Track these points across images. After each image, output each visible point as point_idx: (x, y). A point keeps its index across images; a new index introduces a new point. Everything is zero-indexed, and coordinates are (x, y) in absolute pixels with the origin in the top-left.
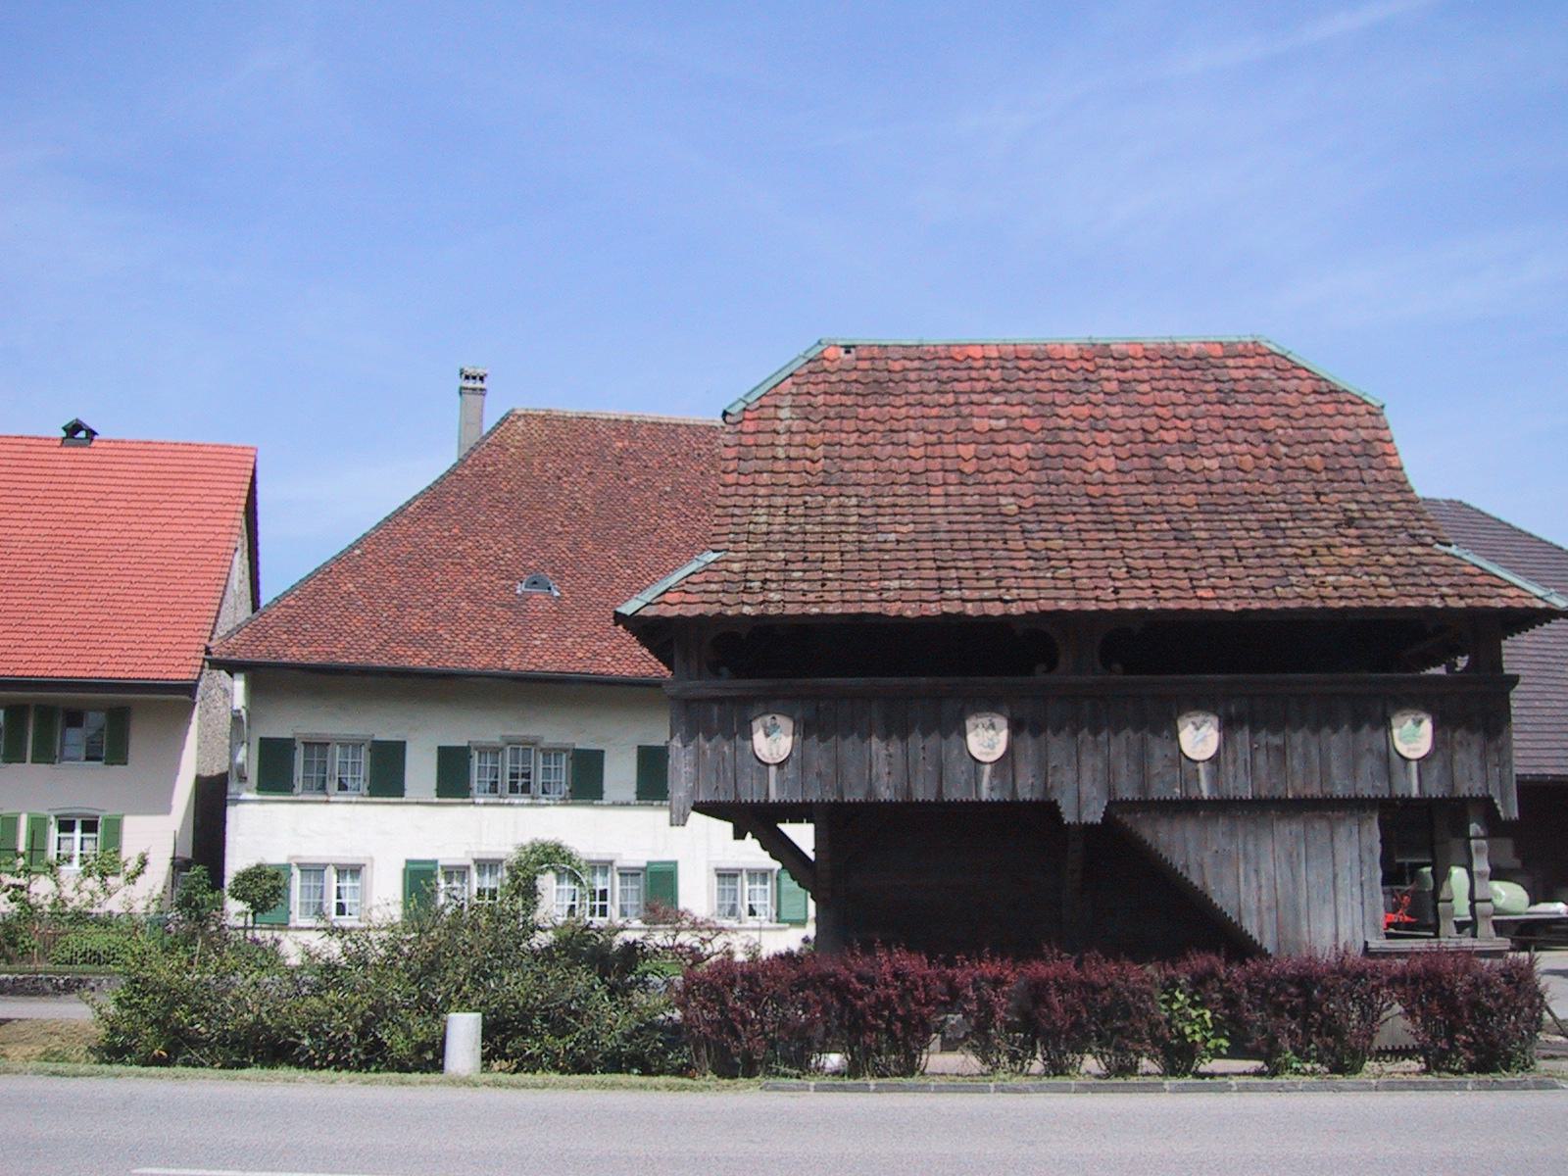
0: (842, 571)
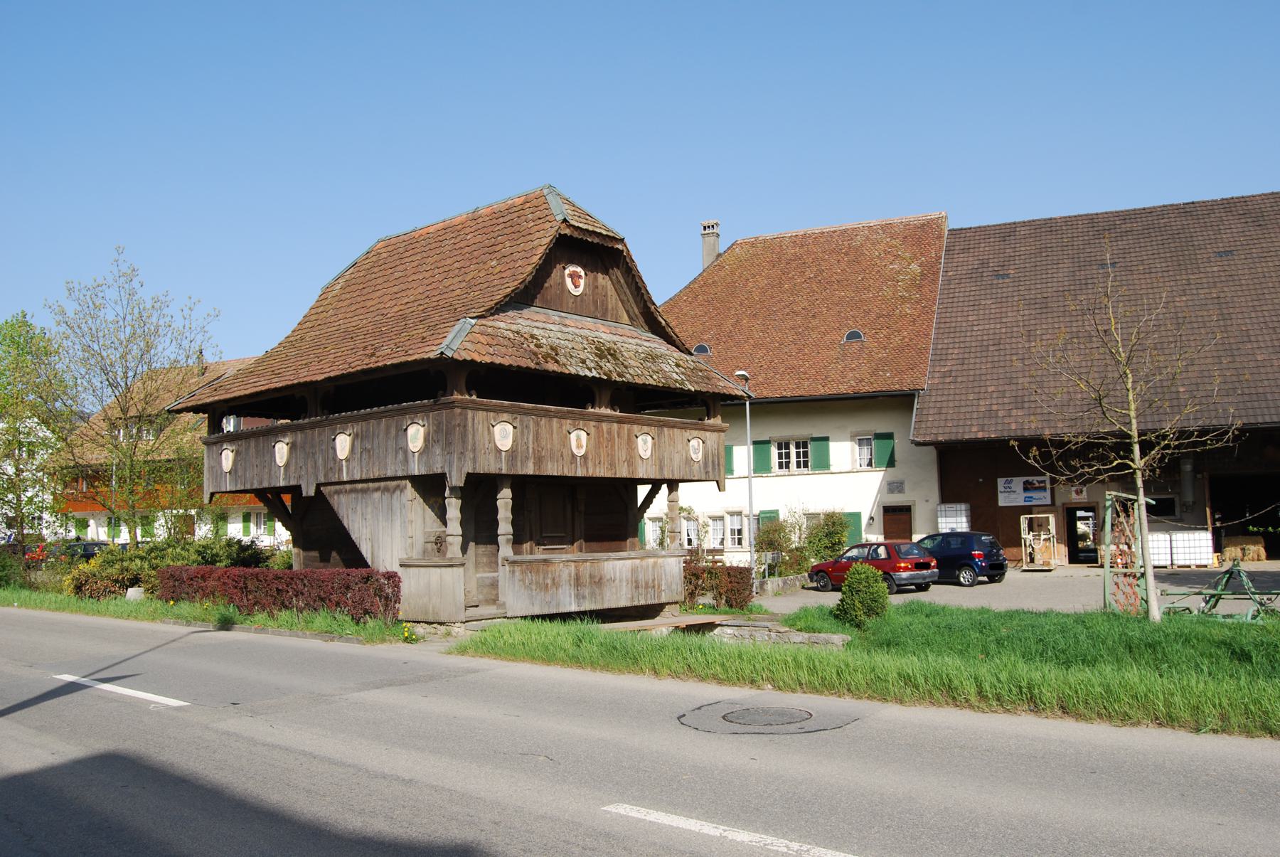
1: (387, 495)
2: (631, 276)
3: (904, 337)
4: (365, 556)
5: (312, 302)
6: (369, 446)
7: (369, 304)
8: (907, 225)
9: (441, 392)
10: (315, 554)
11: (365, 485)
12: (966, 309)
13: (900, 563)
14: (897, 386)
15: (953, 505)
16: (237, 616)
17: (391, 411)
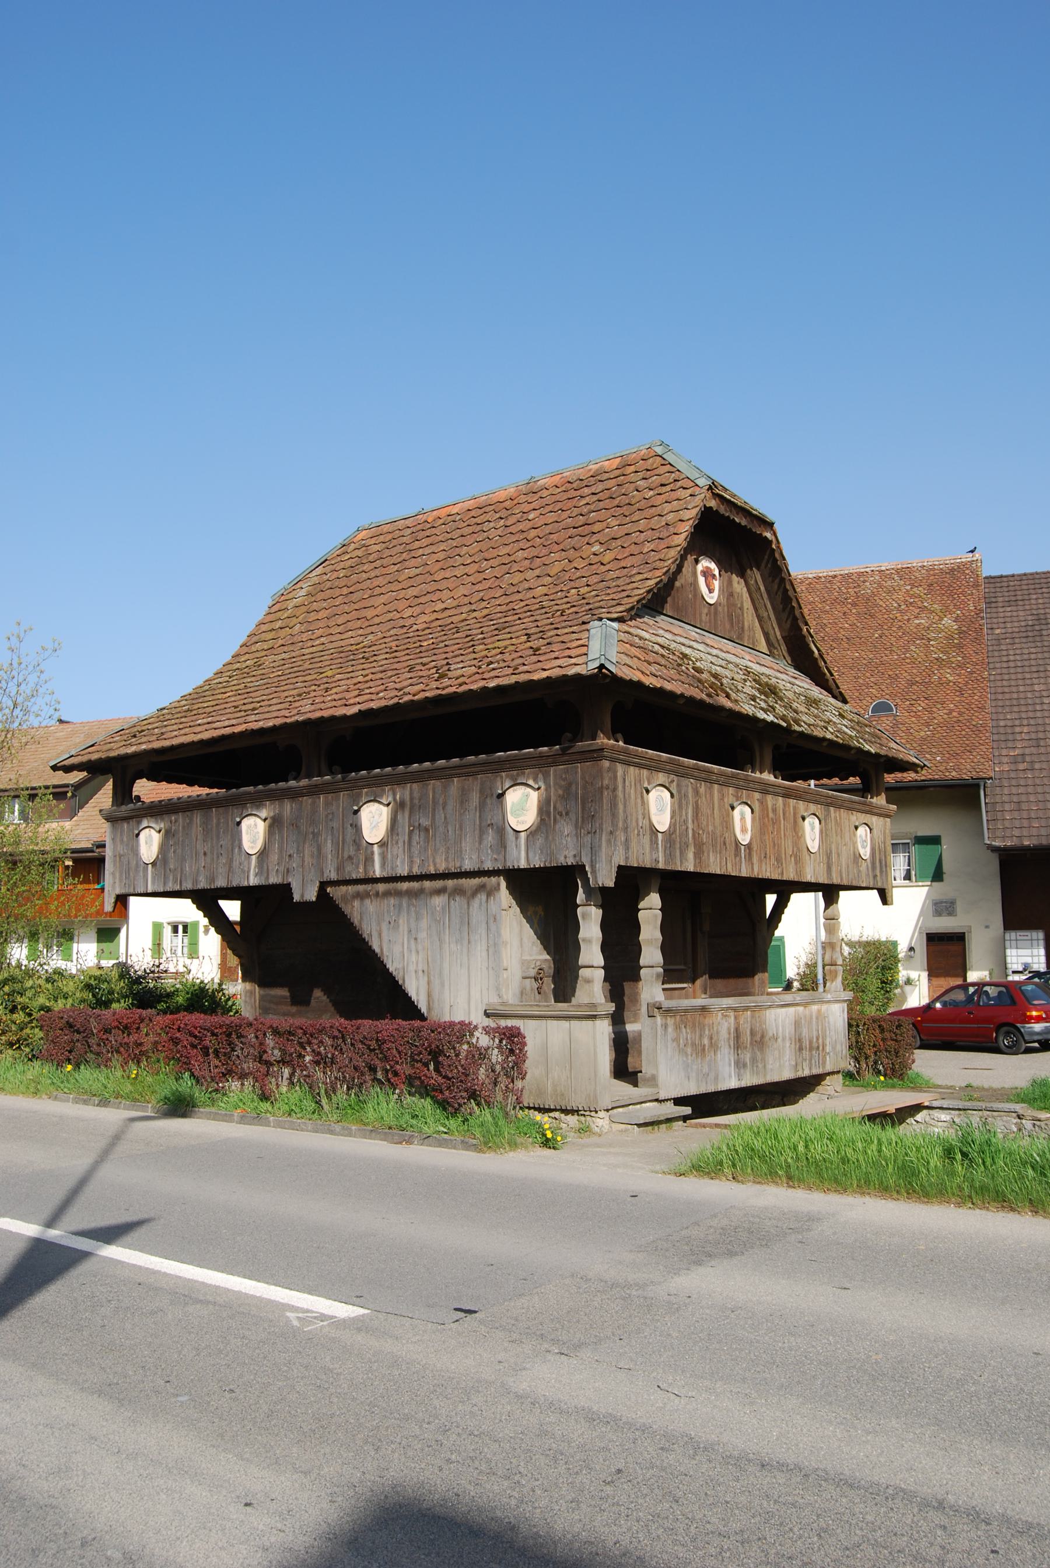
0: (473, 646)
1: (459, 902)
2: (777, 581)
3: (951, 711)
4: (414, 998)
5: (260, 616)
6: (425, 822)
7: (369, 613)
8: (930, 569)
9: (569, 735)
10: (283, 992)
11: (415, 885)
12: (1028, 676)
13: (1030, 1011)
14: (954, 774)
15: (1028, 933)
16: (198, 1093)
17: (474, 765)
